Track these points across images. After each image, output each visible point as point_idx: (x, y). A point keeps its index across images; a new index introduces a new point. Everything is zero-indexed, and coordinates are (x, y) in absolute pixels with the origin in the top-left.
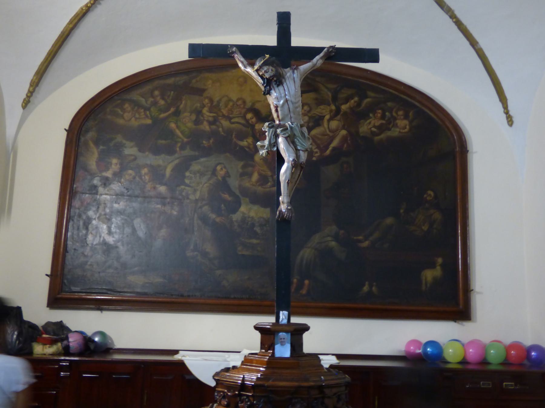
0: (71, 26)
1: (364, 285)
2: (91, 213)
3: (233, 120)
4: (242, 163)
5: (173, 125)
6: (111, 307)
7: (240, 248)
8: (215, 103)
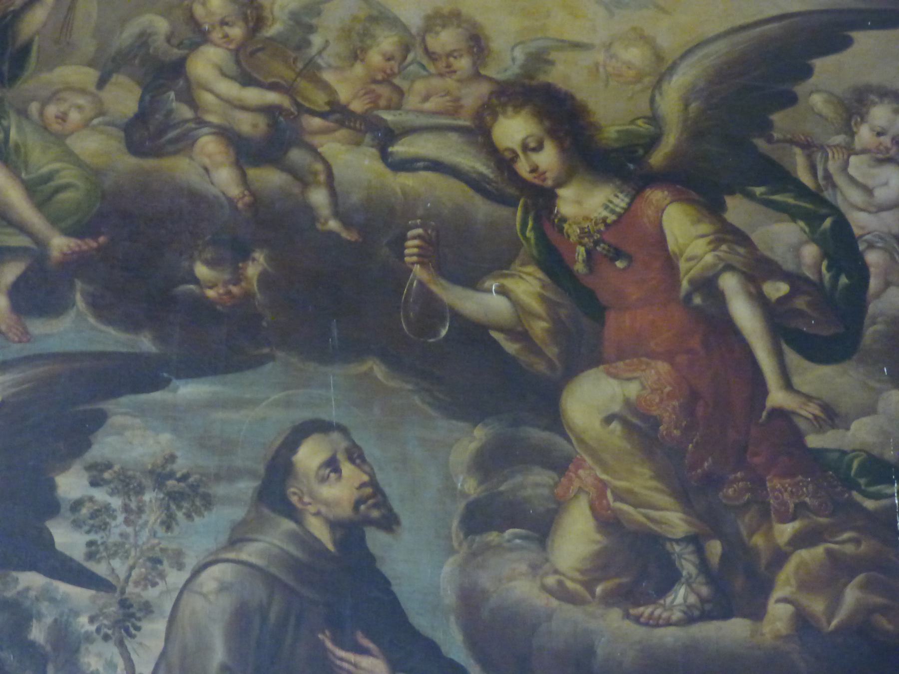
3: (401, 149)
4: (473, 438)
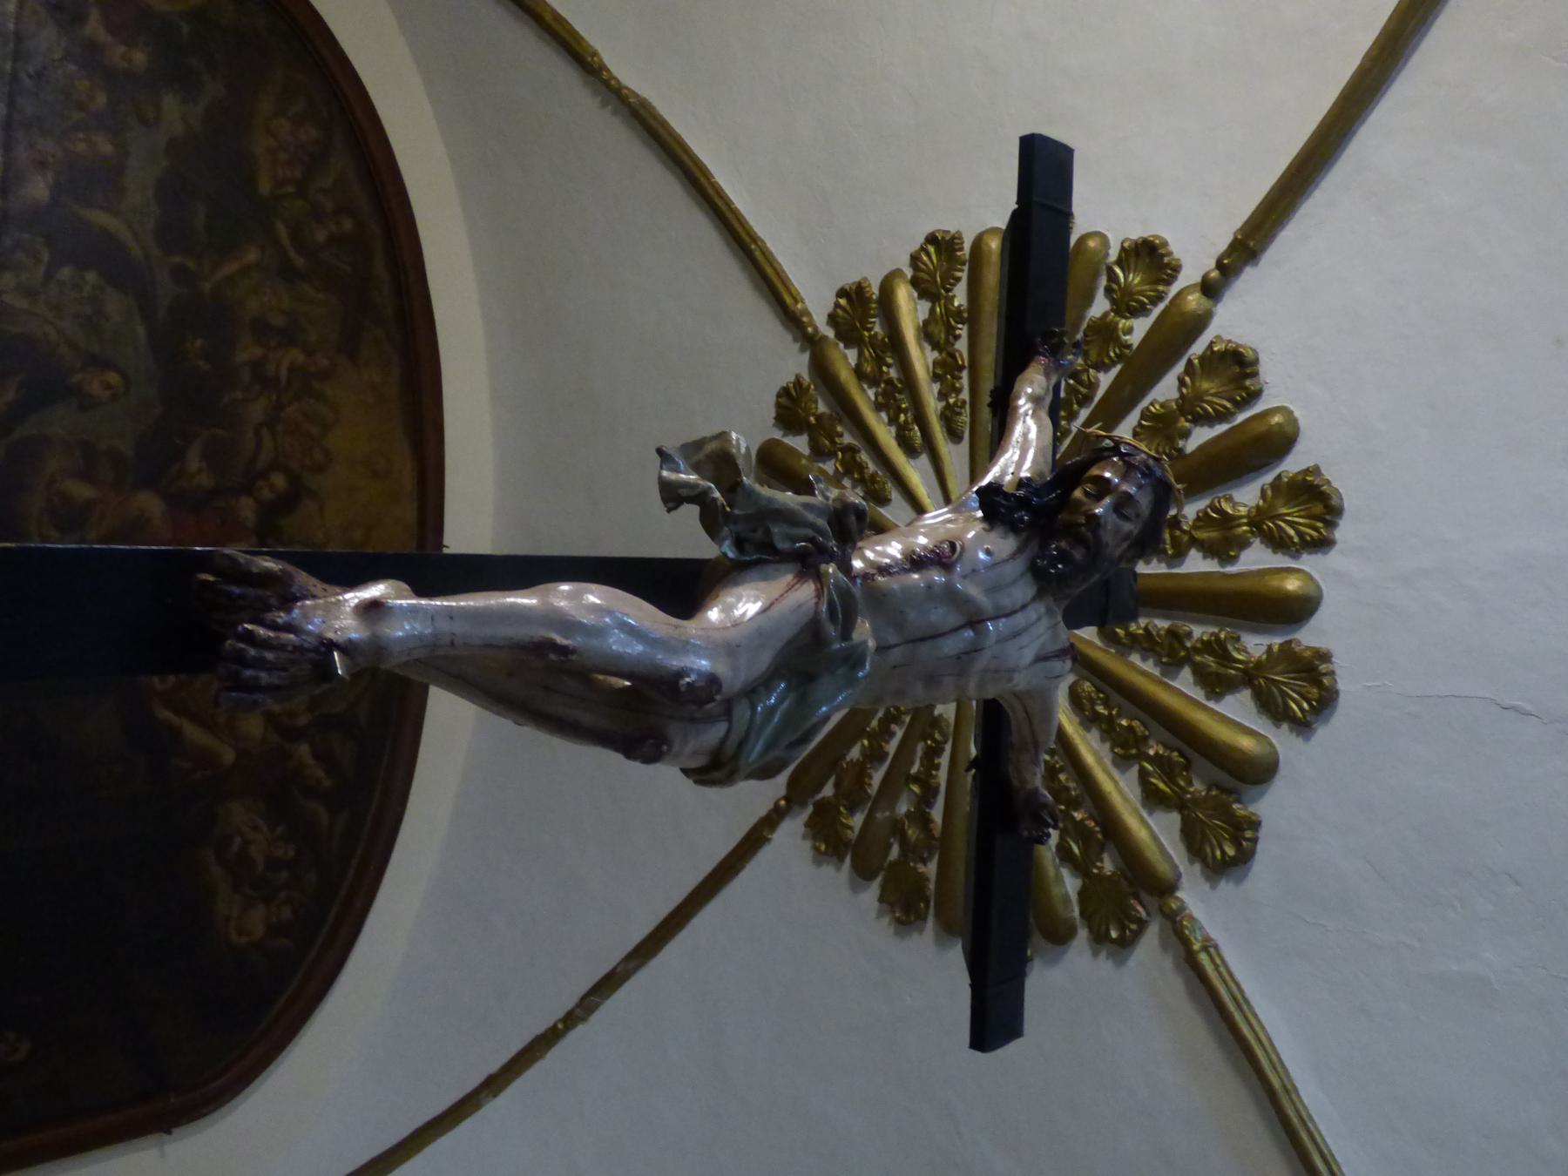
0: (548, 17)
3: (265, 431)
5: (252, 256)
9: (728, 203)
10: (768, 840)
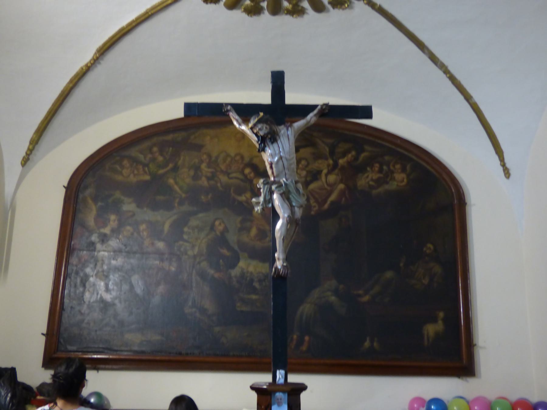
0: (71, 85)
1: (366, 340)
2: (88, 270)
3: (231, 176)
4: (239, 219)
5: (171, 181)
6: (107, 366)
7: (238, 304)
8: (213, 159)
9: (133, 21)
10: (380, 6)
